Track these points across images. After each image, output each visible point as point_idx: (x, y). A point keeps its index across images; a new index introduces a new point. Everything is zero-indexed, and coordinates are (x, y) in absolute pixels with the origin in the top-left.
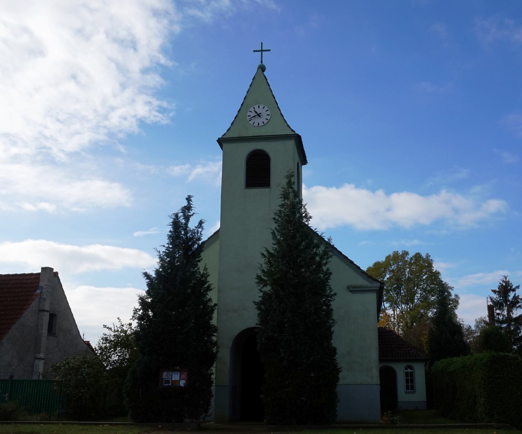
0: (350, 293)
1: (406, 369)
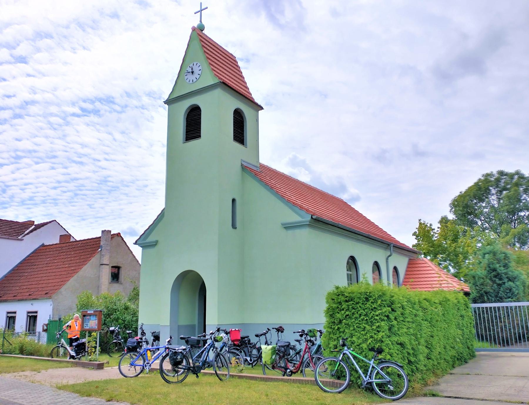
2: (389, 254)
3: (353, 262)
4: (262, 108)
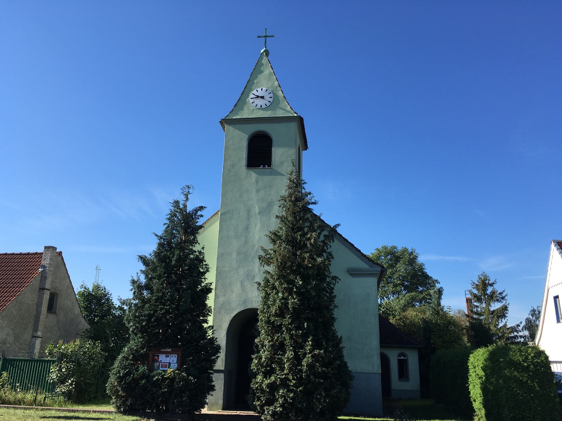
0: (350, 277)
1: (400, 356)
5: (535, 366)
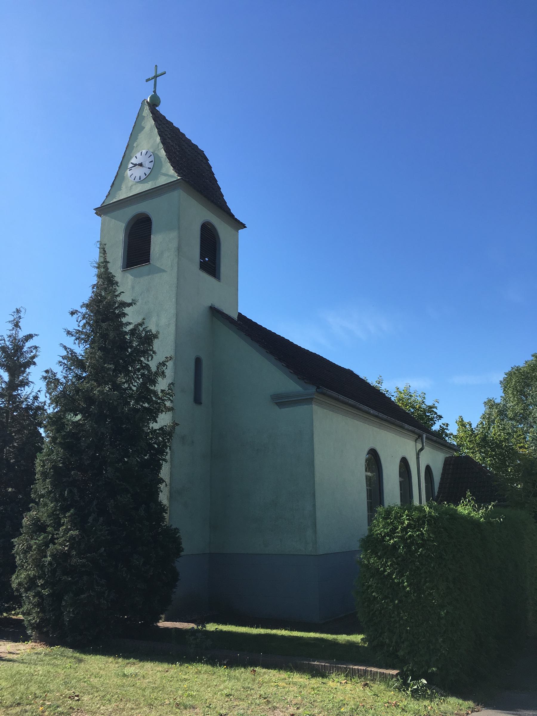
2: (419, 446)
3: (374, 460)
4: (243, 226)
5: (408, 546)
